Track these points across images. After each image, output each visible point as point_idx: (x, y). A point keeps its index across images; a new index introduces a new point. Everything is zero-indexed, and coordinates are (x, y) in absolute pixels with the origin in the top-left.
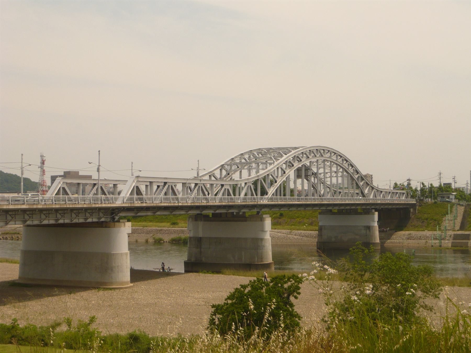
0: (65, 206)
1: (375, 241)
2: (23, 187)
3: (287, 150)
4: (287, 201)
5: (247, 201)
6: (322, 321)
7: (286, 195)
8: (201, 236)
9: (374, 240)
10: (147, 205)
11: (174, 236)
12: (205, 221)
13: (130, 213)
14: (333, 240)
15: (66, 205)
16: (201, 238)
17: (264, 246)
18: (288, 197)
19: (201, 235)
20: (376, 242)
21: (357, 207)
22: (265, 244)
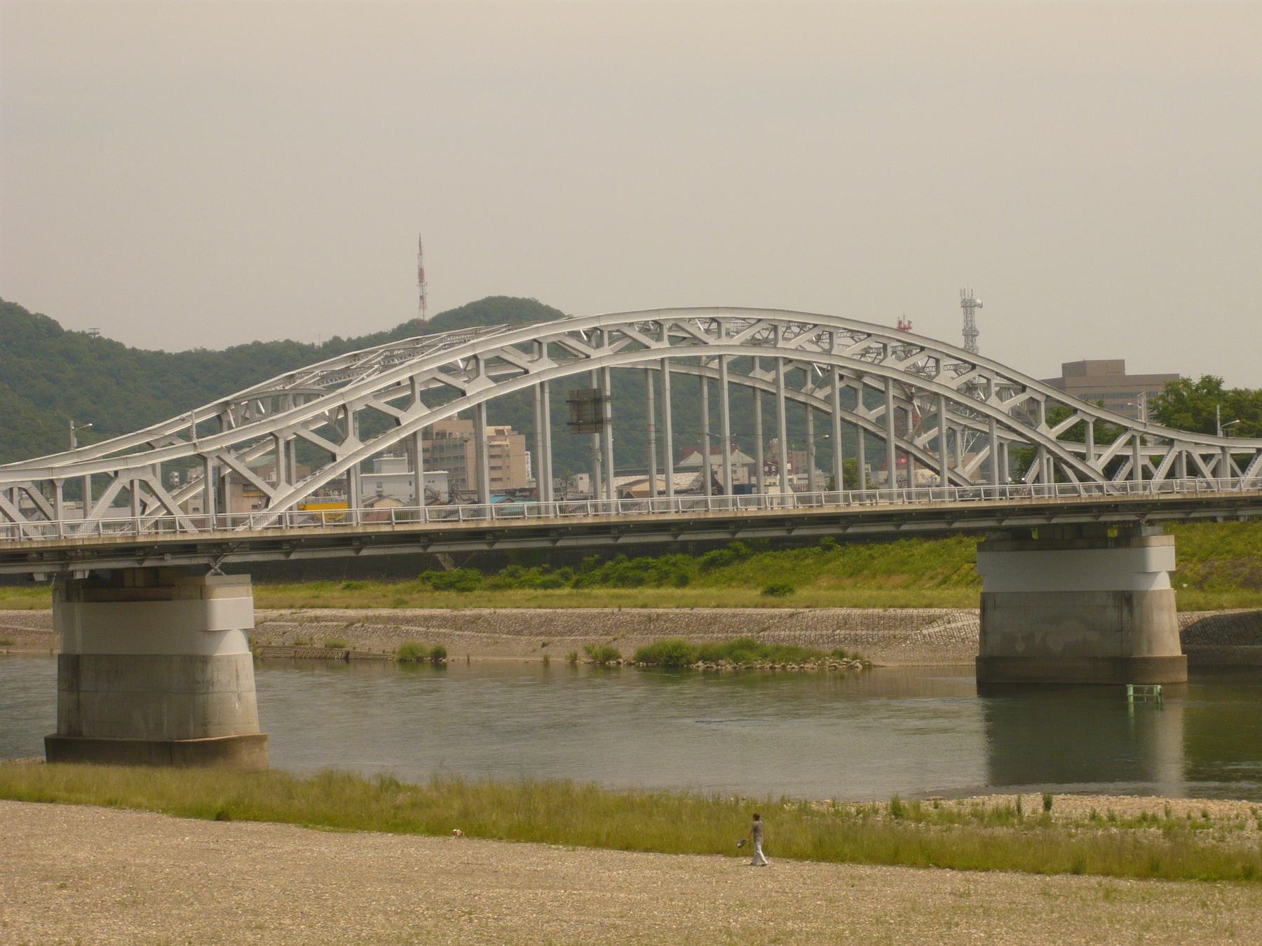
0: (1079, 501)
1: (1150, 650)
2: (551, 429)
3: (551, 314)
4: (524, 518)
5: (525, 517)
6: (909, 906)
7: (1177, 475)
8: (81, 653)
9: (1145, 648)
10: (865, 510)
11: (648, 641)
12: (88, 600)
13: (11, 566)
14: (1020, 647)
15: (1031, 501)
16: (78, 656)
17: (211, 683)
18: (841, 491)
19: (79, 650)
20: (1166, 654)
21: (430, 550)
22: (215, 674)
